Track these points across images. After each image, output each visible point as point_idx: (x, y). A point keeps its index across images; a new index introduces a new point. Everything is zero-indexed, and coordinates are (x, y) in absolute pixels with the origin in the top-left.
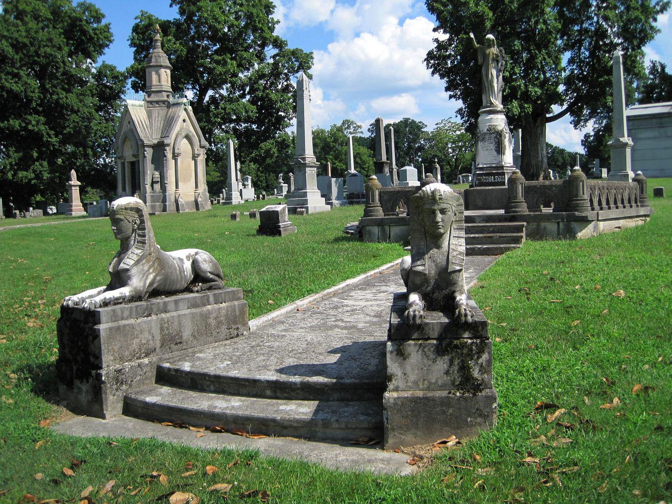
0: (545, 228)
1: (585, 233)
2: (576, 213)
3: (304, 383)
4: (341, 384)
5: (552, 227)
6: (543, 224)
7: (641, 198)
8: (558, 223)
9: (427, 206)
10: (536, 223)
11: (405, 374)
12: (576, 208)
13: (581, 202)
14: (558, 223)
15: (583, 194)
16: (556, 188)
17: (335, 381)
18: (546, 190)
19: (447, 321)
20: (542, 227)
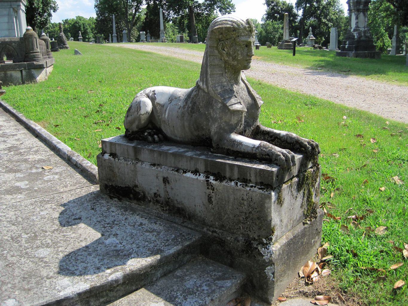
0: (11, 76)
1: (41, 77)
2: (35, 63)
3: (128, 275)
4: (166, 257)
5: (16, 74)
6: (9, 73)
7: (47, 52)
8: (21, 71)
9: (243, 39)
10: (3, 72)
11: (281, 221)
12: (34, 58)
13: (37, 54)
14: (21, 71)
15: (37, 48)
16: (15, 43)
17: (158, 257)
18: (8, 46)
19: (302, 156)
20: (9, 75)
